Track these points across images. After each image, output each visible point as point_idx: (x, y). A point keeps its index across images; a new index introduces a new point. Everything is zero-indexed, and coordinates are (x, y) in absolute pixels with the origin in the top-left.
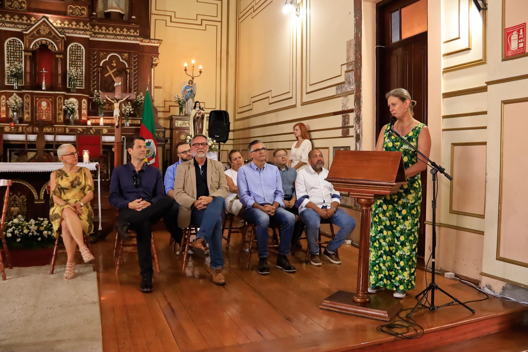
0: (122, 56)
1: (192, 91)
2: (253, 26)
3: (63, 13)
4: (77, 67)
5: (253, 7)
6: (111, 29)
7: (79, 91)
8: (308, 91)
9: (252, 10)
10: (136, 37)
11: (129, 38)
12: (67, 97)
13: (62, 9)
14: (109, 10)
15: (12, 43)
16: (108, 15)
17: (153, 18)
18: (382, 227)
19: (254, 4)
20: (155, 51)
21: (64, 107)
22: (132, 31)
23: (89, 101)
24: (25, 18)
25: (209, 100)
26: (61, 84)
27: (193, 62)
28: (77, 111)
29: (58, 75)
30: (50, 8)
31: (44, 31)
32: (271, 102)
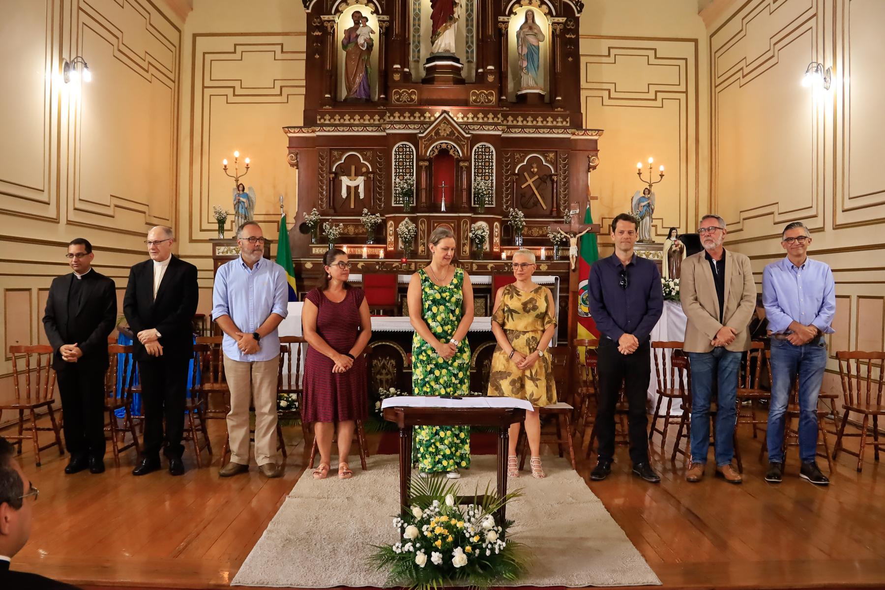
0: (545, 157)
1: (649, 205)
2: (742, 103)
3: (464, 103)
4: (484, 175)
5: (742, 69)
6: (530, 119)
7: (489, 211)
8: (846, 207)
9: (740, 74)
10: (565, 128)
11: (552, 129)
12: (474, 221)
13: (462, 97)
14: (524, 92)
15: (401, 150)
16: (522, 99)
17: (583, 94)
18: (433, 366)
19: (742, 64)
20: (592, 148)
21: (471, 235)
22: (559, 119)
23: (502, 223)
24: (417, 114)
25: (672, 213)
26: (464, 203)
27: (651, 160)
28: (487, 240)
29: (462, 191)
30: (445, 96)
31: (445, 131)
32: (777, 220)
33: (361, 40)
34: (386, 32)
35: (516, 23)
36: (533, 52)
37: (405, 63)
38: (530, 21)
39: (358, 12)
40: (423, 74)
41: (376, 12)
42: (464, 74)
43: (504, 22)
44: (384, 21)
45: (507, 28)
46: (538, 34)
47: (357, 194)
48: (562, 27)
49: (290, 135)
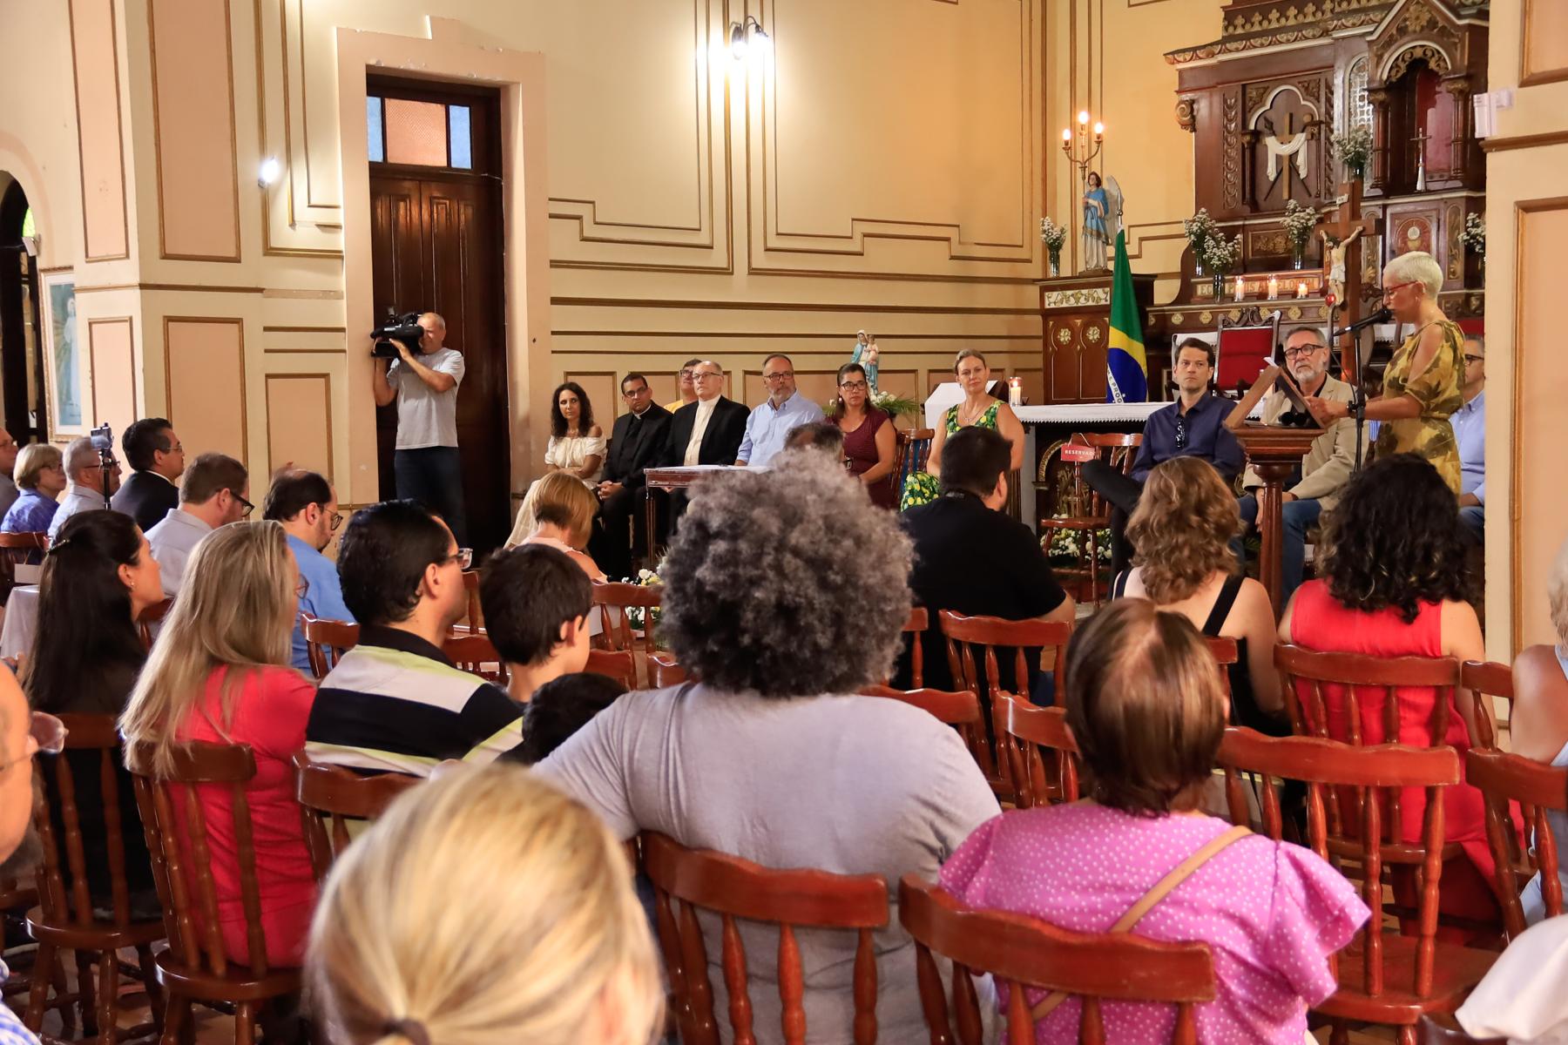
47: (1293, 169)
49: (1180, 66)
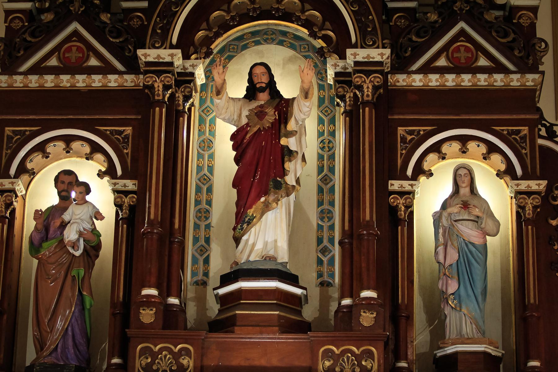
14: (450, 350)
33: (70, 234)
34: (130, 218)
35: (431, 195)
36: (471, 259)
37: (169, 283)
38: (465, 190)
39: (69, 173)
40: (214, 308)
41: (110, 172)
42: (309, 312)
43: (402, 194)
44: (126, 193)
45: (409, 207)
46: (483, 218)
48: (537, 201)
